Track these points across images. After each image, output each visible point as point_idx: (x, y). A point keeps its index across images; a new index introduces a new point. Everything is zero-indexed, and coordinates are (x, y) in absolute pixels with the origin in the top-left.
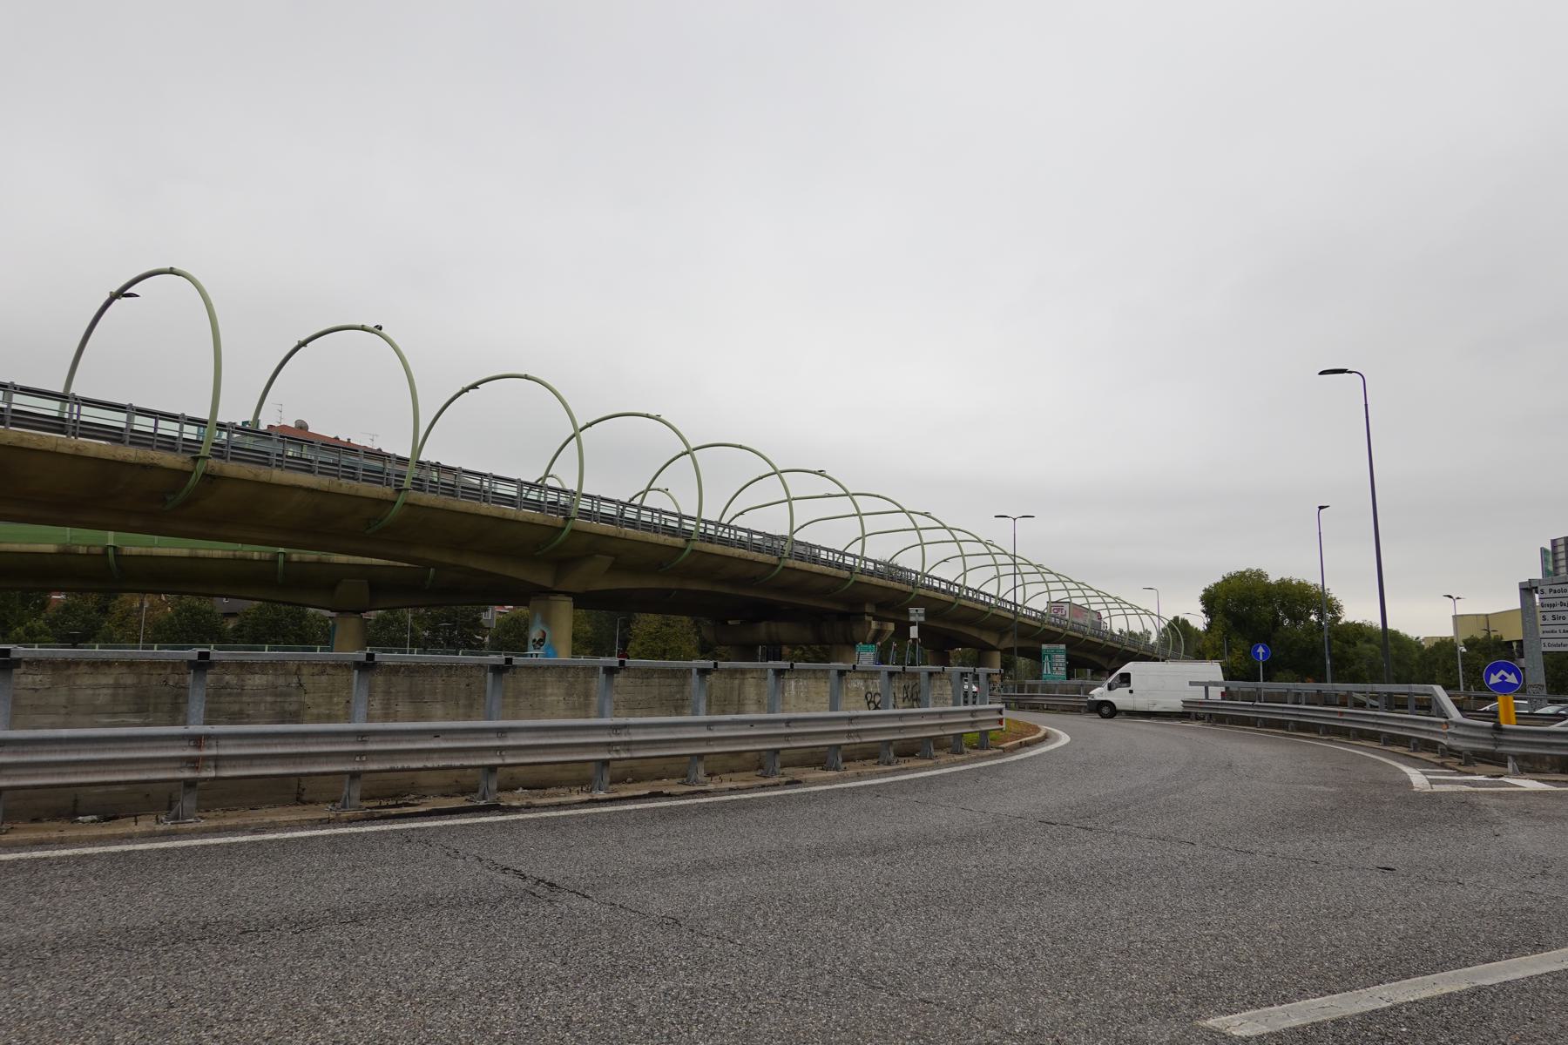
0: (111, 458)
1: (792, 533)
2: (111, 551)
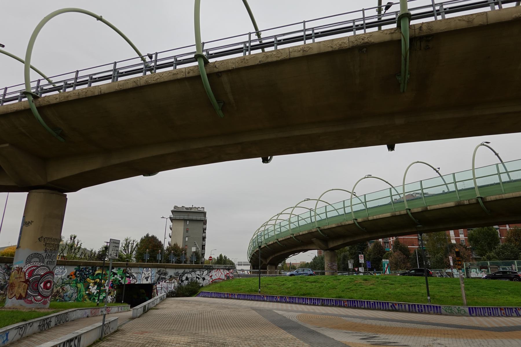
0: (330, 49)
1: (362, 203)
2: (480, 200)
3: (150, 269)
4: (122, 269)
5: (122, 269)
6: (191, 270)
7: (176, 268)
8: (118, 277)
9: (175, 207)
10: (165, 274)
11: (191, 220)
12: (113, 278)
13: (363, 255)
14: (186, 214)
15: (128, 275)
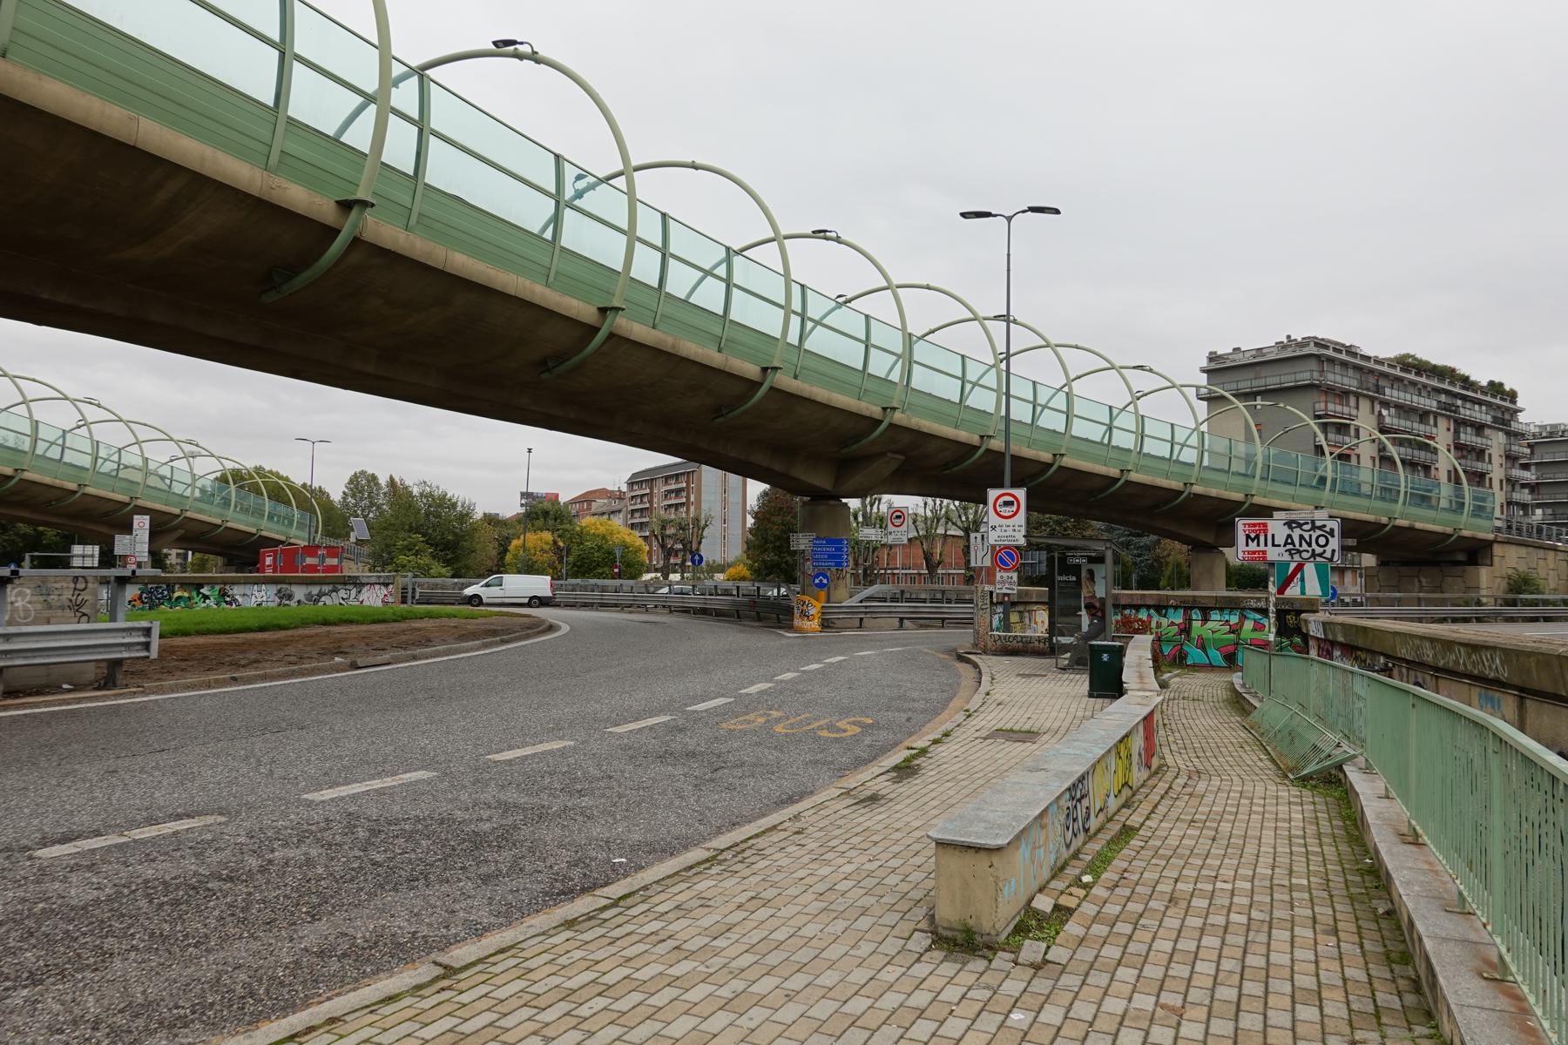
3: (263, 587)
4: (217, 588)
5: (217, 588)
6: (331, 587)
7: (307, 584)
8: (212, 604)
9: (1213, 357)
10: (290, 597)
11: (1266, 393)
12: (203, 605)
13: (1021, 494)
14: (1250, 374)
15: (228, 599)
